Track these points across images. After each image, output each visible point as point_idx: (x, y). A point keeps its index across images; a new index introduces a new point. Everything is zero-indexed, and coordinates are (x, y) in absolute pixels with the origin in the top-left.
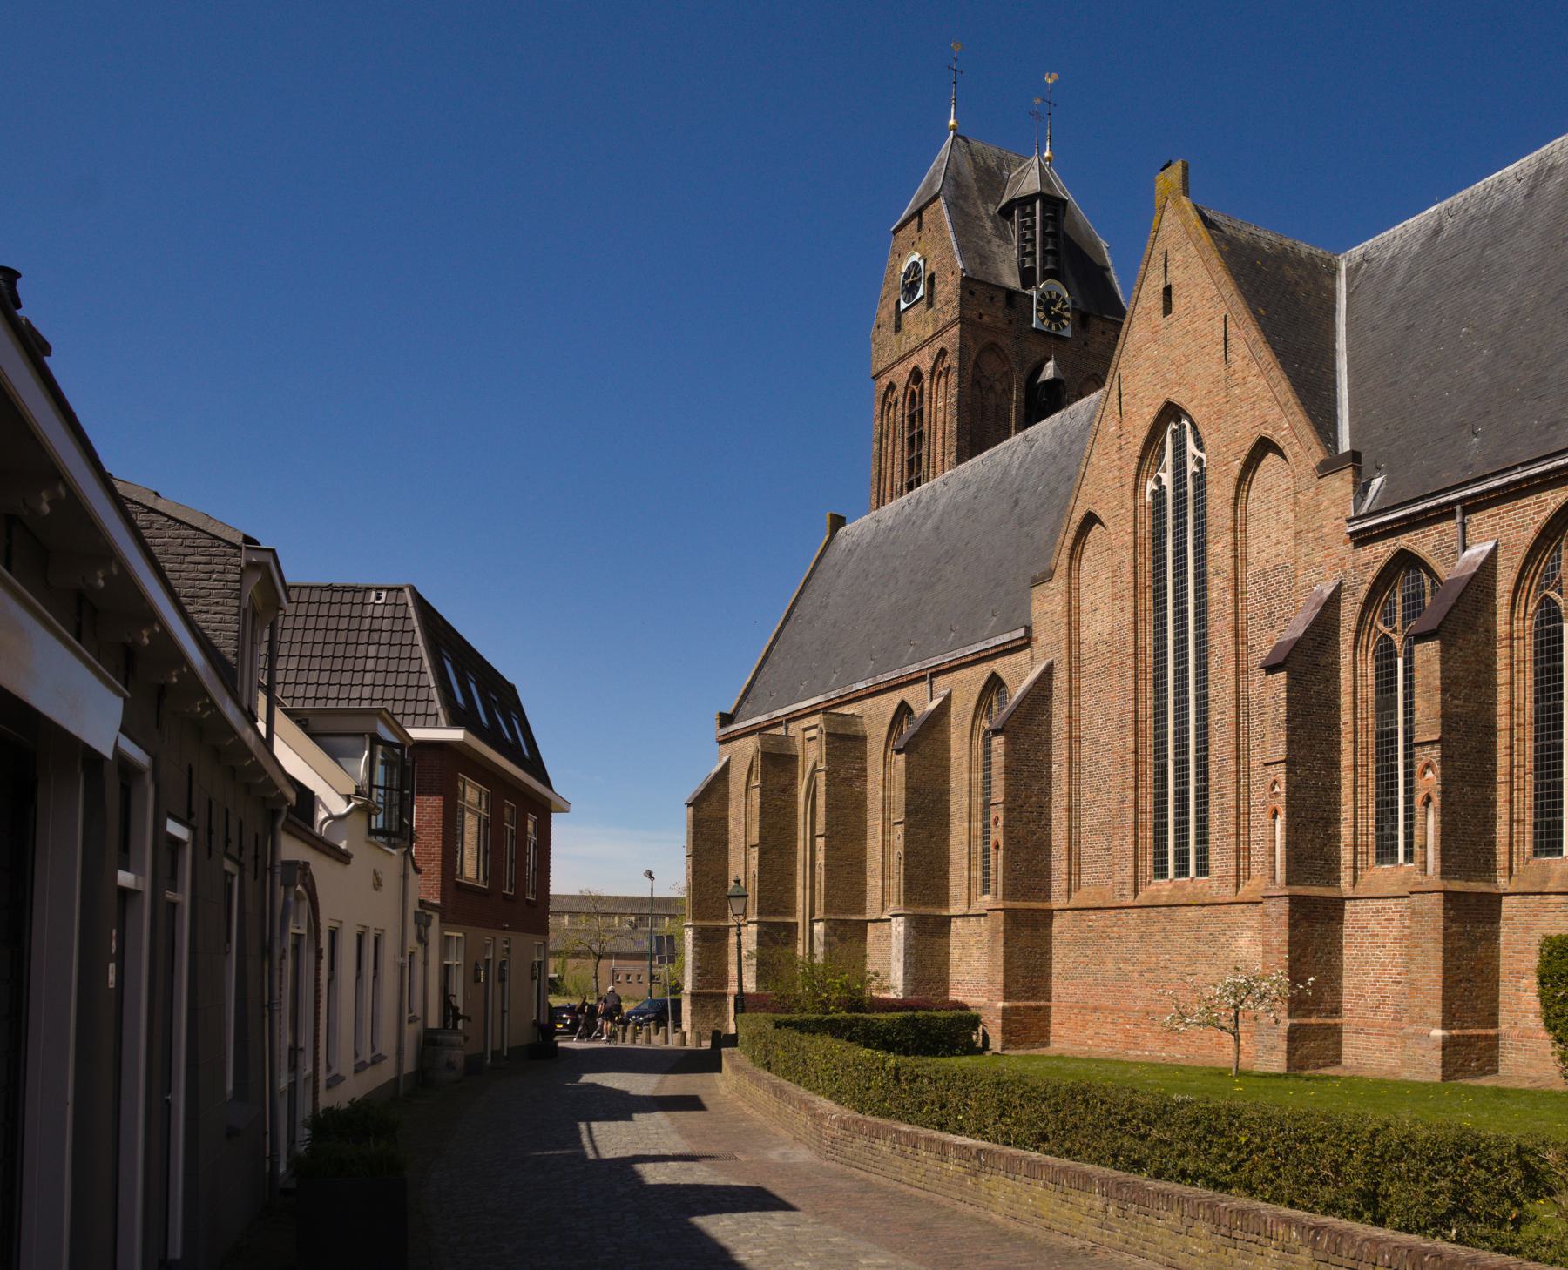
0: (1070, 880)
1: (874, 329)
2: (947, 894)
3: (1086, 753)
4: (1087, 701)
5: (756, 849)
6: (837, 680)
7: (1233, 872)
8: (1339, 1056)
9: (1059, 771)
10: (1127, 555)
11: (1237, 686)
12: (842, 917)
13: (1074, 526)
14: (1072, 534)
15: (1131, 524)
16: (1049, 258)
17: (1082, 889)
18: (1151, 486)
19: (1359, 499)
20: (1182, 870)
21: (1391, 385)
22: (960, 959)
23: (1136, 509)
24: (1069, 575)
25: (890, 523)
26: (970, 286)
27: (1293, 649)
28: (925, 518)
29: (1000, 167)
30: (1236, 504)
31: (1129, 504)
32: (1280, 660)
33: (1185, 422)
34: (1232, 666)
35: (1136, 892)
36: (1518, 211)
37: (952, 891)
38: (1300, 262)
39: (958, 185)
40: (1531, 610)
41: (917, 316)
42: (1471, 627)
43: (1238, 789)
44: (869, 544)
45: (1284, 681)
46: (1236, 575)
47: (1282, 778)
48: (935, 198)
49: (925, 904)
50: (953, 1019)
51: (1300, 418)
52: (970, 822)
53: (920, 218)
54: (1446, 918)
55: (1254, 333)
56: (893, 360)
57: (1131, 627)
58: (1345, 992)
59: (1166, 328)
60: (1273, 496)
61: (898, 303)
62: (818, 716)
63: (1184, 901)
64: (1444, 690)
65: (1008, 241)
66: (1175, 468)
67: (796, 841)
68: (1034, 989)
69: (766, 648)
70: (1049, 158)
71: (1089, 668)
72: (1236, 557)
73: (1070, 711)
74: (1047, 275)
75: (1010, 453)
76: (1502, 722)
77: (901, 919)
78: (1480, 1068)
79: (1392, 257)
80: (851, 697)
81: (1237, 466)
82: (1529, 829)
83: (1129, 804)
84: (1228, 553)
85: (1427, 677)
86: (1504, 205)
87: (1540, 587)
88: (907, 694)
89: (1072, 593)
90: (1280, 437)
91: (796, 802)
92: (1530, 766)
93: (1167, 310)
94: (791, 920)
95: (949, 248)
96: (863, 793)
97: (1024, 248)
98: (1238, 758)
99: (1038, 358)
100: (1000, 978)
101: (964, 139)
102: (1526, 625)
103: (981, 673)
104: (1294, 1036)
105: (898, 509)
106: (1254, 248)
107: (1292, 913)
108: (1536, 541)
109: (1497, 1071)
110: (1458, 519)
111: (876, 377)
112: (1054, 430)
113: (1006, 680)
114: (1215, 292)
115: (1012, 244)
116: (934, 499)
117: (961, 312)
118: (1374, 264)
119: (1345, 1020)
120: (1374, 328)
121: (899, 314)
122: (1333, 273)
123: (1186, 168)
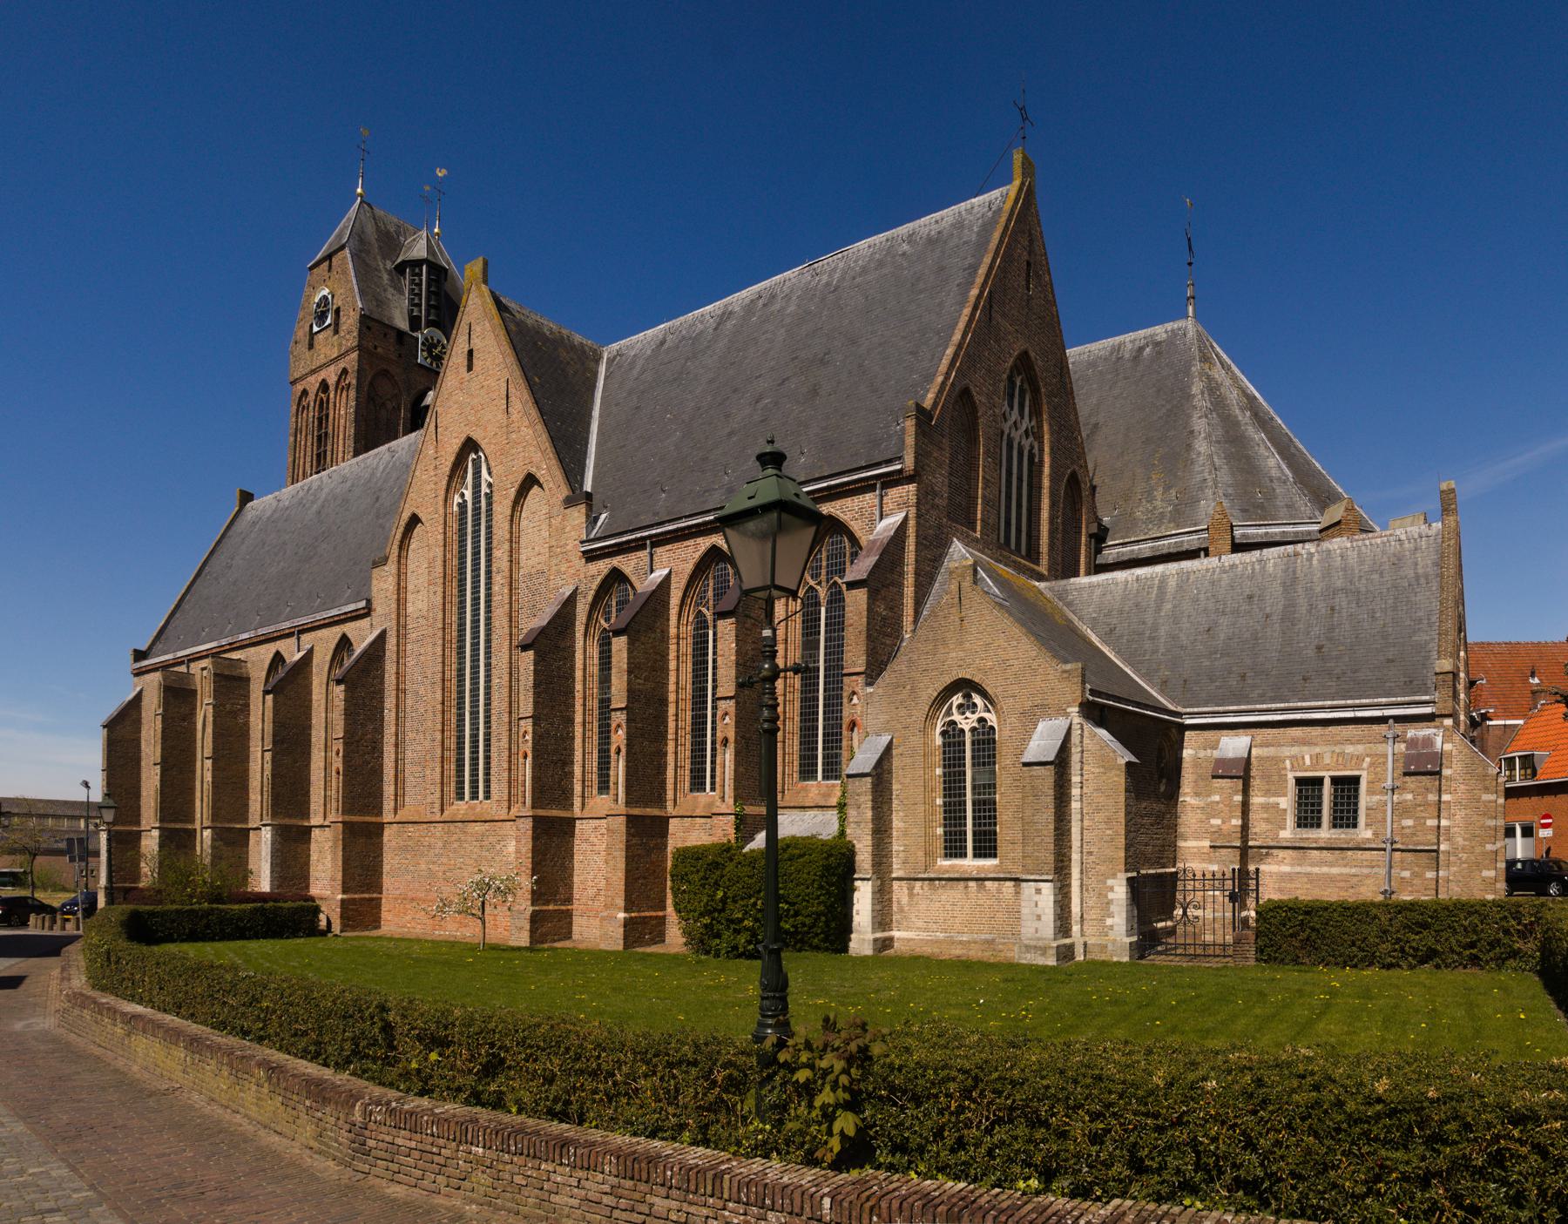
0: (396, 800)
1: (292, 344)
2: (309, 808)
3: (409, 702)
4: (411, 661)
5: (159, 767)
6: (231, 630)
7: (506, 798)
8: (570, 932)
9: (389, 715)
10: (439, 551)
11: (511, 658)
12: (227, 825)
13: (403, 523)
14: (401, 530)
15: (442, 526)
16: (432, 311)
17: (406, 807)
19: (590, 528)
20: (474, 796)
21: (621, 447)
22: (318, 861)
23: (446, 516)
24: (399, 562)
25: (287, 503)
26: (370, 324)
27: (539, 634)
28: (313, 502)
29: (398, 234)
30: (512, 521)
31: (441, 511)
32: (529, 641)
33: (481, 454)
34: (507, 643)
35: (442, 811)
36: (709, 338)
37: (313, 807)
38: (572, 347)
39: (362, 241)
40: (691, 619)
41: (327, 339)
42: (651, 629)
43: (510, 736)
44: (268, 518)
45: (532, 658)
46: (511, 575)
47: (530, 729)
48: (342, 248)
49: (290, 816)
50: (297, 908)
51: (554, 462)
52: (326, 752)
54: (628, 834)
55: (526, 395)
56: (307, 371)
57: (441, 607)
58: (575, 886)
59: (469, 381)
60: (537, 519)
61: (311, 326)
62: (206, 660)
63: (472, 818)
64: (630, 672)
65: (401, 292)
67: (195, 761)
68: (368, 884)
69: (179, 597)
70: (438, 234)
71: (412, 636)
72: (511, 561)
73: (398, 669)
74: (429, 324)
75: (378, 459)
76: (672, 697)
77: (269, 828)
78: (652, 940)
79: (634, 356)
80: (238, 645)
81: (513, 492)
82: (687, 772)
83: (438, 743)
84: (506, 558)
85: (619, 662)
86: (702, 332)
87: (697, 605)
88: (281, 646)
89: (401, 576)
90: (541, 475)
91: (195, 729)
92: (689, 729)
93: (470, 368)
94: (190, 827)
95: (352, 289)
96: (247, 724)
97: (413, 299)
98: (510, 712)
99: (421, 387)
100: (339, 876)
101: (369, 205)
102: (688, 630)
103: (333, 634)
104: (535, 919)
105: (294, 492)
106: (537, 332)
107: (535, 828)
108: (694, 572)
109: (664, 941)
110: (648, 550)
111: (293, 383)
112: (410, 445)
113: (352, 640)
114: (501, 360)
115: (404, 294)
116: (320, 488)
117: (359, 341)
118: (624, 358)
119: (574, 907)
120: (616, 405)
121: (312, 335)
122: (597, 360)
123: (486, 264)
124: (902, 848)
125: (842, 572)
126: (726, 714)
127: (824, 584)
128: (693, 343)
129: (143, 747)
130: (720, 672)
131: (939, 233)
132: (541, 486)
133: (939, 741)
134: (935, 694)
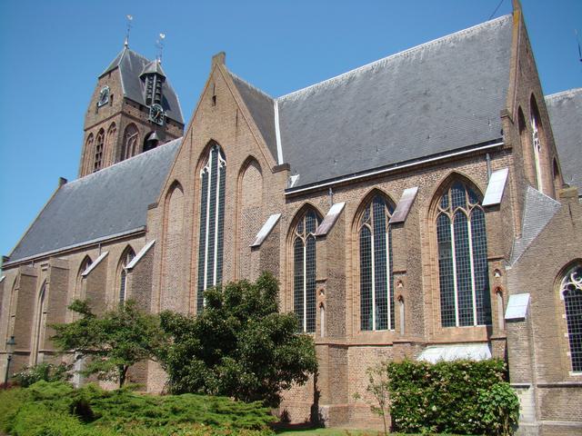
13: (169, 185)
18: (202, 172)
66: (213, 165)
89: (122, 297)
102: (356, 236)
103: (81, 256)
116: (106, 175)
122: (273, 103)
124: (542, 366)
125: (314, 230)
127: (451, 211)
128: (335, 92)
129: (3, 307)
130: (396, 257)
132: (182, 190)
133: (562, 297)
134: (560, 269)
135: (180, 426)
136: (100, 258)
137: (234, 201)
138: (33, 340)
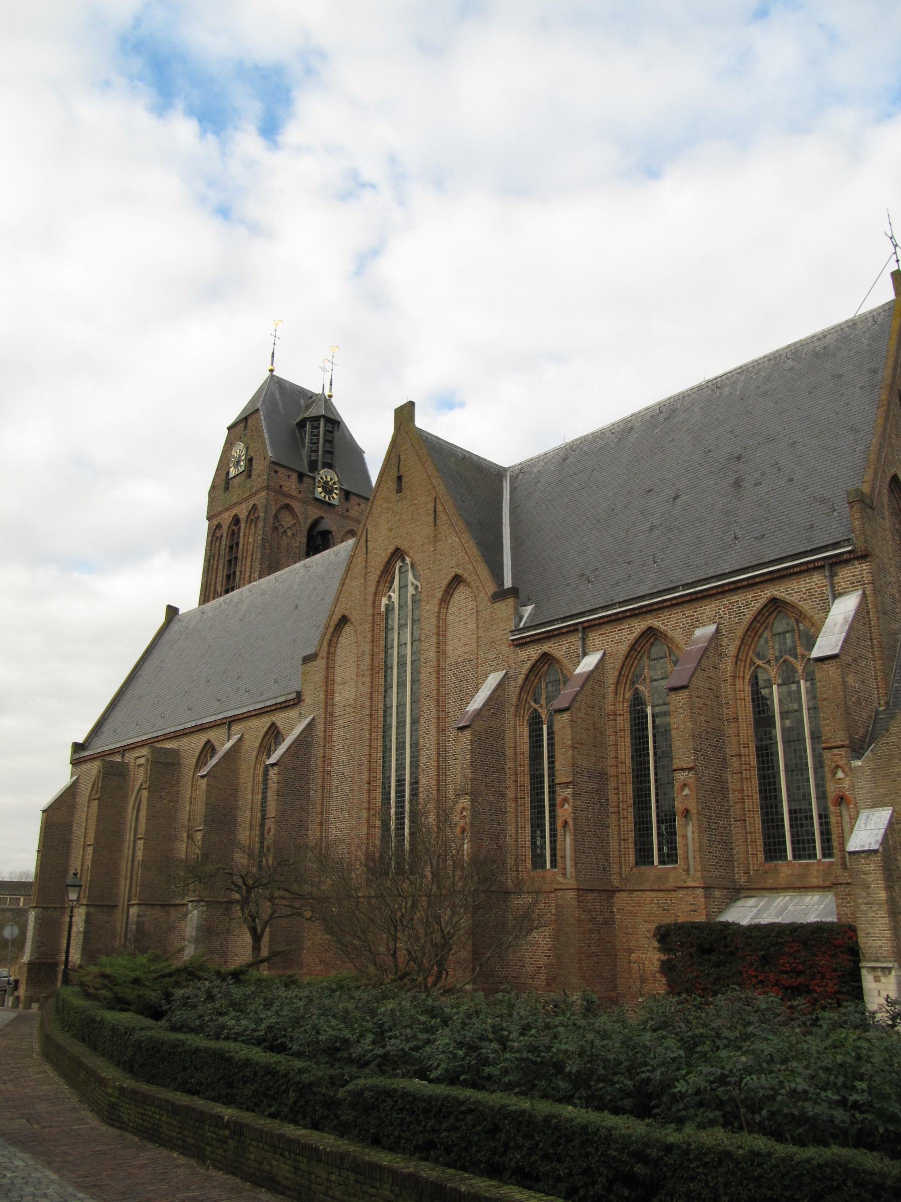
53: (246, 422)
93: (399, 490)
116: (241, 601)
126: (685, 785)
131: (825, 348)
132: (468, 585)
135: (545, 1168)
136: (228, 745)
137: (434, 649)
138: (124, 886)
